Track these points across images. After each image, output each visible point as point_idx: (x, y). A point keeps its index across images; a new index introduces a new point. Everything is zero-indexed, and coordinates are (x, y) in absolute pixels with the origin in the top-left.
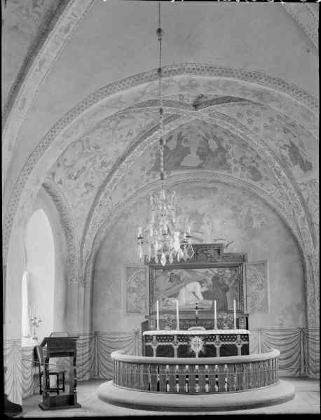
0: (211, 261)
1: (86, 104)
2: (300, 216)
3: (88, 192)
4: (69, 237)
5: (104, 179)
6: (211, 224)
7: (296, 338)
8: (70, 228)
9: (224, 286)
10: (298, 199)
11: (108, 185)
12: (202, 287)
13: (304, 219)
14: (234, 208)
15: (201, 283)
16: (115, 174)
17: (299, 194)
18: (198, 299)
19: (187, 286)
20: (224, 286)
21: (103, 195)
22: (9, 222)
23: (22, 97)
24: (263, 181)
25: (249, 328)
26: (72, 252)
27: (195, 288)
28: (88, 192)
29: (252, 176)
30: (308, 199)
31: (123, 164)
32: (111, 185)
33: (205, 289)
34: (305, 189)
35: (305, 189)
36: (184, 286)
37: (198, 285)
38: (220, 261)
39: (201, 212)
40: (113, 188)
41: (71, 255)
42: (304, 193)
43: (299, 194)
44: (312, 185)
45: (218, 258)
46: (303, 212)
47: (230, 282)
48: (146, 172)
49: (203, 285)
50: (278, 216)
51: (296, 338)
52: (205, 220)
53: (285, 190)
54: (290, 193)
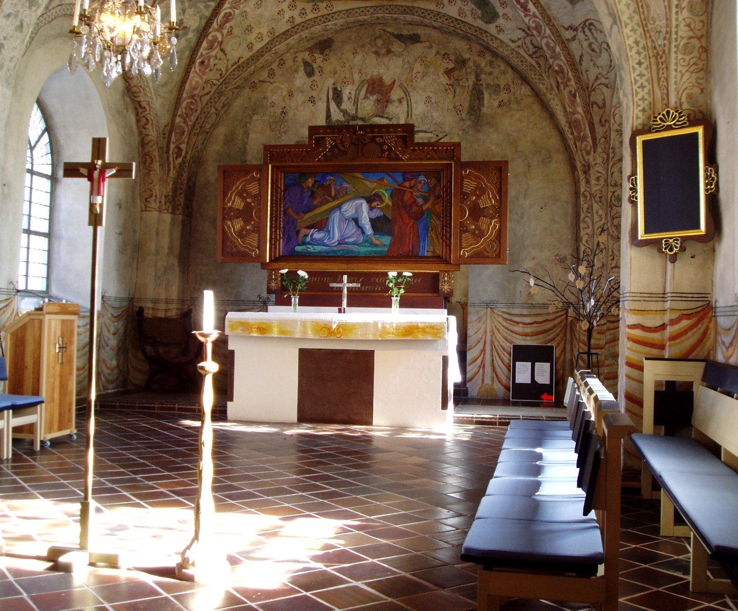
0: (390, 159)
2: (568, 89)
4: (144, 120)
5: (207, 14)
6: (405, 102)
7: (556, 322)
8: (144, 104)
9: (415, 209)
10: (563, 58)
12: (371, 209)
13: (574, 96)
14: (448, 72)
15: (369, 201)
17: (565, 48)
18: (363, 233)
19: (345, 207)
20: (415, 209)
21: (205, 44)
24: (501, 21)
26: (148, 149)
27: (358, 209)
29: (479, 12)
30: (581, 57)
32: (221, 27)
33: (377, 213)
34: (574, 39)
35: (574, 39)
36: (339, 207)
37: (365, 206)
38: (406, 160)
39: (387, 81)
40: (225, 32)
42: (574, 46)
43: (565, 48)
44: (586, 30)
45: (403, 153)
46: (573, 82)
47: (426, 200)
49: (374, 204)
50: (532, 89)
51: (556, 322)
52: (395, 95)
53: (539, 39)
54: (547, 44)
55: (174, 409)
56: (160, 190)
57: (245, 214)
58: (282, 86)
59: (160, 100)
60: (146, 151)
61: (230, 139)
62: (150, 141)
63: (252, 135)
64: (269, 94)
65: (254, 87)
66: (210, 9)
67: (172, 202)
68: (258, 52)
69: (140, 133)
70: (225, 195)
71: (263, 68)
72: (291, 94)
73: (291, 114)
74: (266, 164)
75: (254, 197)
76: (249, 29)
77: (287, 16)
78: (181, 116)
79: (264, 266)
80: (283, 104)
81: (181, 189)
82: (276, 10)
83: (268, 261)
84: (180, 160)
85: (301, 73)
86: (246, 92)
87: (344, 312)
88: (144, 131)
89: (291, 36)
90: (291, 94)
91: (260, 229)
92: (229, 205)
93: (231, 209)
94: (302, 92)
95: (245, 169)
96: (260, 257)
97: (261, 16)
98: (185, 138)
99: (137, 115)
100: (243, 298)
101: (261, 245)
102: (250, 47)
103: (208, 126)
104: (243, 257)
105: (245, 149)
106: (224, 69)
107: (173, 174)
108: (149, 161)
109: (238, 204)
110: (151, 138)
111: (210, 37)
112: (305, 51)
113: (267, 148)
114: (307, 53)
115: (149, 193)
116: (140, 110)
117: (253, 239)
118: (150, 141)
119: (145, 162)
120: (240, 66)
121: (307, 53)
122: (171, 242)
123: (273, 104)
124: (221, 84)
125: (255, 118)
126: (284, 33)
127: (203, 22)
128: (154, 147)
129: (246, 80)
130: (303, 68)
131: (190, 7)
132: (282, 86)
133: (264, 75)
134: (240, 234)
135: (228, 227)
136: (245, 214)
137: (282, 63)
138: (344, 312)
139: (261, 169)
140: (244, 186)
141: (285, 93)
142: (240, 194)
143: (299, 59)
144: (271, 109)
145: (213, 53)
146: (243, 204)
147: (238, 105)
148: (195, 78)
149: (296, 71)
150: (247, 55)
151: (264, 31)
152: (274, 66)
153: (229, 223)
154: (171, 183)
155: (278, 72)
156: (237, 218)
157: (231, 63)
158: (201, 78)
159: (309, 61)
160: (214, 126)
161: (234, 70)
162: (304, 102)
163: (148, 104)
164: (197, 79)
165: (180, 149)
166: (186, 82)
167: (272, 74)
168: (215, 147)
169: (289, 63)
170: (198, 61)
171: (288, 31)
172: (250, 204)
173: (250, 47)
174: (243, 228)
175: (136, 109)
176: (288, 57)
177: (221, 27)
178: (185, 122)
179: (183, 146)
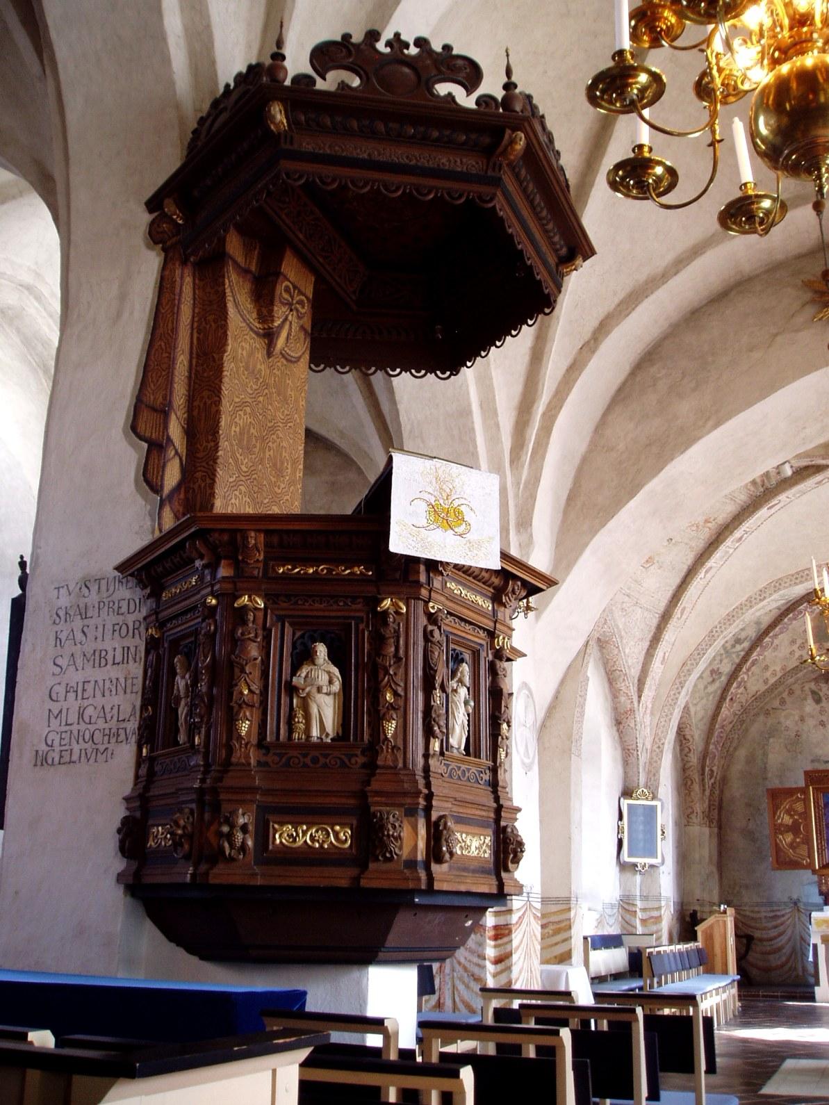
1: (751, 602)
3: (713, 681)
5: (737, 661)
8: (688, 737)
11: (744, 670)
16: (755, 654)
21: (735, 685)
22: (659, 747)
23: (682, 606)
25: (35, 753)
26: (688, 772)
28: (713, 681)
31: (767, 639)
32: (748, 670)
41: (686, 777)
48: (797, 645)
55: (758, 996)
56: (699, 807)
57: (794, 829)
58: (793, 712)
59: (699, 732)
60: (687, 775)
61: (750, 760)
62: (691, 767)
63: (771, 756)
64: (782, 720)
65: (767, 713)
66: (740, 657)
67: (708, 816)
68: (772, 685)
69: (683, 760)
70: (774, 814)
71: (775, 698)
72: (802, 719)
73: (804, 737)
74: (807, 786)
75: (800, 815)
76: (766, 668)
77: (797, 655)
78: (714, 744)
79: (814, 872)
80: (797, 728)
81: (713, 805)
82: (788, 651)
83: (817, 867)
84: (712, 781)
85: (810, 701)
86: (762, 718)
87: (585, 938)
88: (686, 758)
89: (801, 671)
90: (802, 719)
91: (808, 841)
92: (779, 821)
93: (781, 824)
94: (813, 717)
95: (790, 792)
96: (810, 866)
97: (776, 656)
98: (716, 761)
99: (681, 746)
100: (775, 900)
101: (811, 855)
102: (766, 682)
103: (731, 749)
104: (795, 865)
105: (765, 768)
106: (744, 701)
107: (707, 793)
108: (689, 783)
109: (787, 820)
110: (691, 764)
111: (739, 679)
112: (810, 681)
113: (807, 773)
114: (813, 683)
115: (690, 810)
116: (684, 742)
117: (803, 850)
118: (691, 767)
119: (686, 785)
120: (758, 698)
121: (813, 683)
122: (710, 852)
123: (787, 729)
124: (742, 714)
125: (771, 740)
126: (793, 669)
127: (734, 666)
128: (695, 771)
129: (762, 708)
130: (810, 697)
131: (726, 657)
132: (793, 712)
133: (776, 703)
134: (791, 845)
135: (780, 840)
136: (794, 829)
137: (791, 692)
138: (585, 938)
139: (804, 791)
140: (791, 805)
141: (797, 718)
142: (788, 812)
143: (806, 688)
144: (786, 733)
145: (739, 691)
146: (791, 821)
147: (755, 730)
148: (725, 712)
149: (805, 699)
150: (763, 688)
151: (778, 668)
152: (785, 695)
153: (781, 837)
154: (707, 800)
155: (788, 700)
156: (787, 832)
157: (750, 696)
158: (729, 711)
159: (817, 690)
160: (735, 749)
161: (753, 701)
162: (815, 726)
163: (692, 736)
164: (727, 712)
165: (712, 771)
166: (718, 716)
167: (783, 702)
168: (738, 766)
169: (798, 692)
170: (729, 698)
171: (797, 667)
172: (797, 820)
173: (766, 682)
174: (793, 841)
175: (681, 741)
176: (796, 687)
177: (748, 670)
178: (716, 748)
179: (715, 769)
